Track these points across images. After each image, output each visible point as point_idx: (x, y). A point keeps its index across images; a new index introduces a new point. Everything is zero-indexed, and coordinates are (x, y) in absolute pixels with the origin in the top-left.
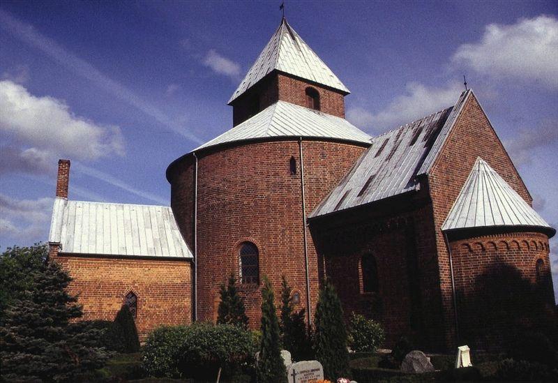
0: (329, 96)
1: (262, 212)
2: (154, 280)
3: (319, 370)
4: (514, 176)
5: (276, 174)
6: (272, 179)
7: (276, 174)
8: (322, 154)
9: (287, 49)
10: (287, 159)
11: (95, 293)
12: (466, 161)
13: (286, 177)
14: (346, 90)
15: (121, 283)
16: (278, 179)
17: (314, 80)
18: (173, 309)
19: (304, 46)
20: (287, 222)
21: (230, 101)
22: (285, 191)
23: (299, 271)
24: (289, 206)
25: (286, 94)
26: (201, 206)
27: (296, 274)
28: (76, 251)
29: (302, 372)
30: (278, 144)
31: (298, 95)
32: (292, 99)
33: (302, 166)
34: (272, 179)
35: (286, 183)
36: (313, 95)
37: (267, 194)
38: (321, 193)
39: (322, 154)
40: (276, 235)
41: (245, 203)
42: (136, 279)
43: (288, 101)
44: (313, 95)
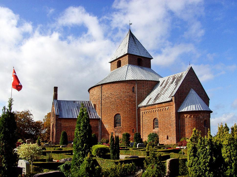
8: (143, 86)
39: (143, 86)
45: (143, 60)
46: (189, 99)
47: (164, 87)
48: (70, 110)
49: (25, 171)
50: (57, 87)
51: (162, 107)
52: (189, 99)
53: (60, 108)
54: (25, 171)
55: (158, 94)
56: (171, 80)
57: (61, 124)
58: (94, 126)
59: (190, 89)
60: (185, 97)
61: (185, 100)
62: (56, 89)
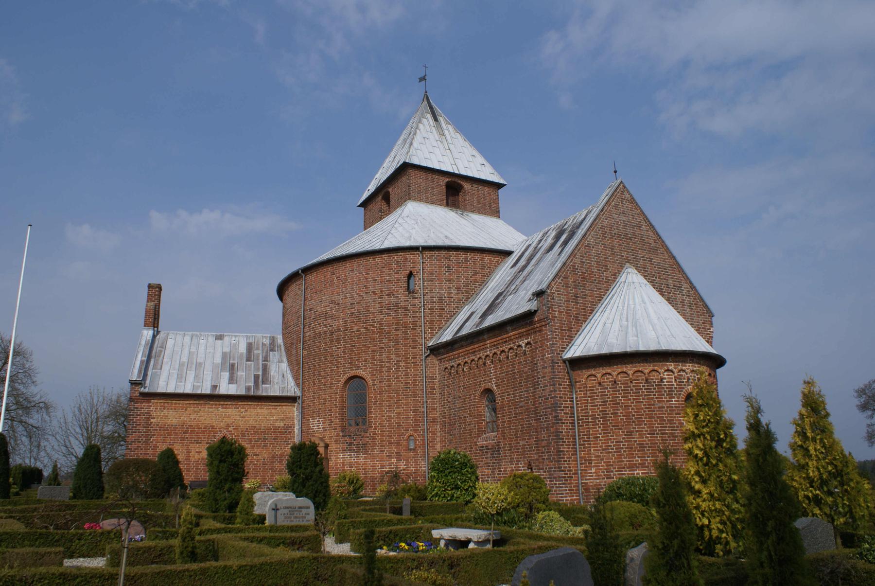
0: (478, 191)
1: (373, 340)
2: (252, 422)
3: (308, 508)
4: (685, 286)
5: (391, 293)
6: (386, 299)
7: (391, 293)
8: (448, 267)
9: (425, 135)
10: (404, 274)
11: (183, 439)
12: (606, 270)
13: (402, 296)
14: (502, 181)
15: (213, 427)
16: (393, 300)
17: (457, 172)
18: (273, 457)
19: (450, 131)
20: (402, 351)
21: (361, 201)
22: (400, 314)
23: (415, 411)
24: (405, 332)
25: (419, 192)
26: (308, 334)
27: (411, 415)
28: (161, 389)
29: (286, 508)
30: (394, 257)
31: (436, 191)
32: (427, 198)
33: (418, 283)
34: (386, 299)
35: (403, 304)
36: (454, 190)
37: (379, 317)
38: (444, 312)
39: (448, 267)
40: (390, 368)
41: (355, 329)
42: (229, 421)
43: (421, 200)
44: (454, 190)
45: (467, 186)
46: (615, 307)
47: (525, 267)
48: (192, 363)
49: (586, 527)
50: (159, 288)
51: (506, 342)
52: (615, 307)
53: (159, 356)
54: (586, 527)
55: (500, 294)
56: (550, 241)
57: (149, 417)
58: (277, 424)
59: (622, 267)
60: (600, 298)
61: (600, 310)
62: (155, 291)
